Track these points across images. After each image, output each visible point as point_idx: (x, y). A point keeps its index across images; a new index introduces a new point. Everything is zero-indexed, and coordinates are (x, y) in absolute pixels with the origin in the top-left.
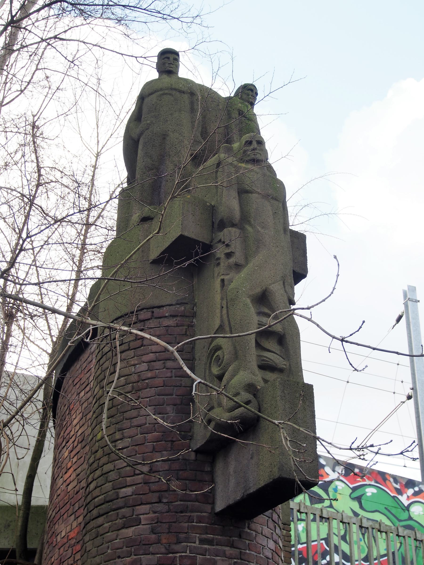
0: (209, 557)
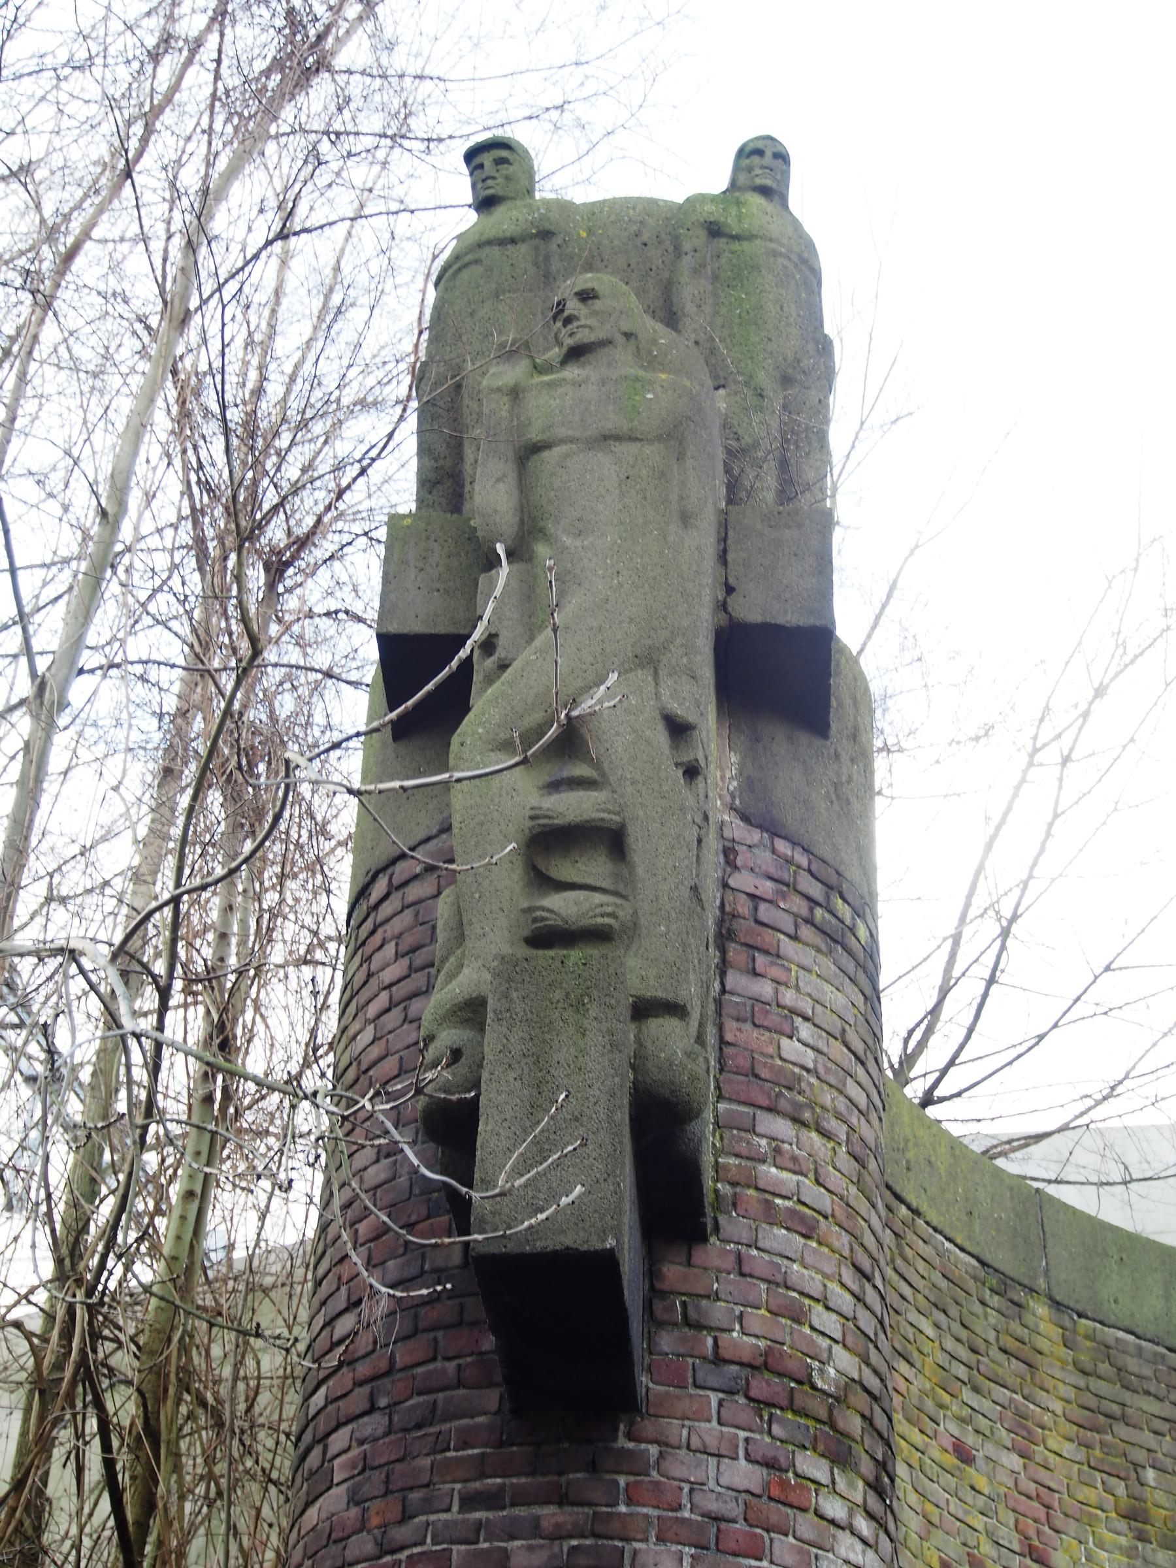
0: (486, 1545)
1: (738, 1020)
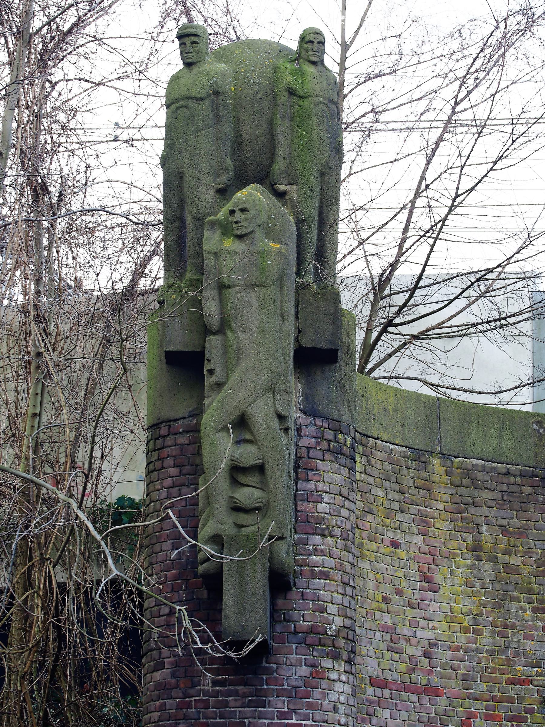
0: (221, 699)
1: (302, 501)
